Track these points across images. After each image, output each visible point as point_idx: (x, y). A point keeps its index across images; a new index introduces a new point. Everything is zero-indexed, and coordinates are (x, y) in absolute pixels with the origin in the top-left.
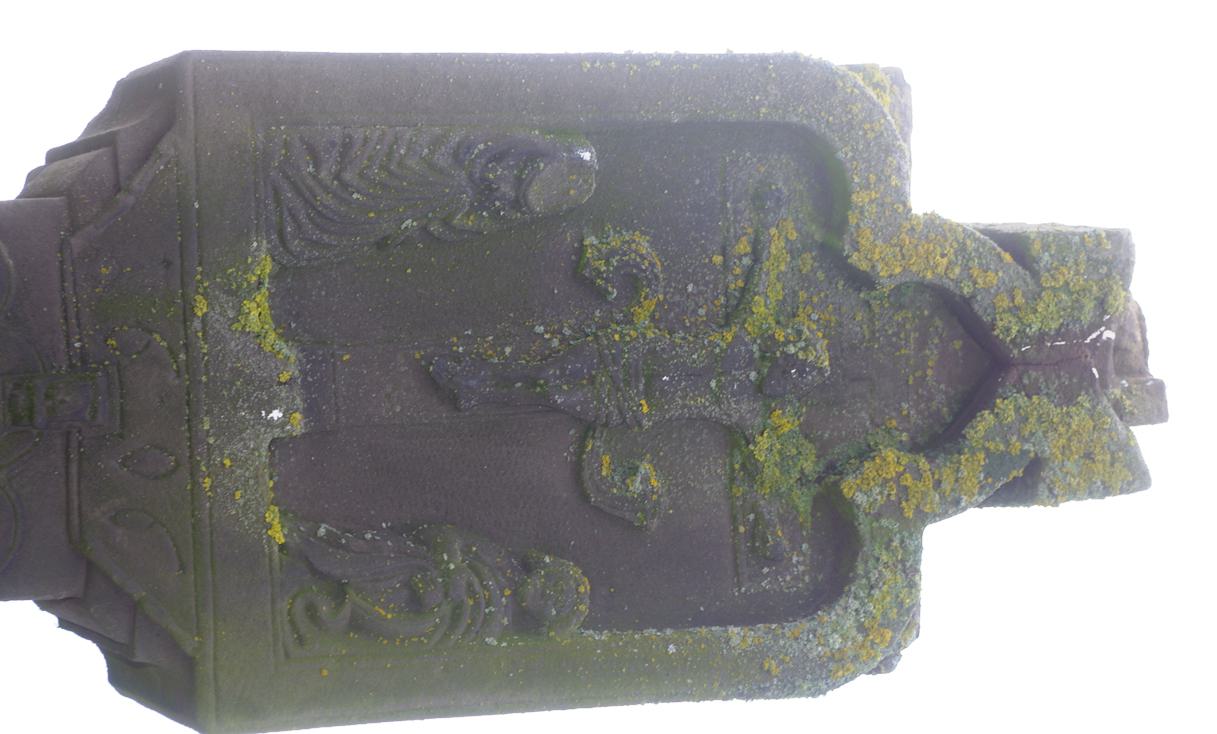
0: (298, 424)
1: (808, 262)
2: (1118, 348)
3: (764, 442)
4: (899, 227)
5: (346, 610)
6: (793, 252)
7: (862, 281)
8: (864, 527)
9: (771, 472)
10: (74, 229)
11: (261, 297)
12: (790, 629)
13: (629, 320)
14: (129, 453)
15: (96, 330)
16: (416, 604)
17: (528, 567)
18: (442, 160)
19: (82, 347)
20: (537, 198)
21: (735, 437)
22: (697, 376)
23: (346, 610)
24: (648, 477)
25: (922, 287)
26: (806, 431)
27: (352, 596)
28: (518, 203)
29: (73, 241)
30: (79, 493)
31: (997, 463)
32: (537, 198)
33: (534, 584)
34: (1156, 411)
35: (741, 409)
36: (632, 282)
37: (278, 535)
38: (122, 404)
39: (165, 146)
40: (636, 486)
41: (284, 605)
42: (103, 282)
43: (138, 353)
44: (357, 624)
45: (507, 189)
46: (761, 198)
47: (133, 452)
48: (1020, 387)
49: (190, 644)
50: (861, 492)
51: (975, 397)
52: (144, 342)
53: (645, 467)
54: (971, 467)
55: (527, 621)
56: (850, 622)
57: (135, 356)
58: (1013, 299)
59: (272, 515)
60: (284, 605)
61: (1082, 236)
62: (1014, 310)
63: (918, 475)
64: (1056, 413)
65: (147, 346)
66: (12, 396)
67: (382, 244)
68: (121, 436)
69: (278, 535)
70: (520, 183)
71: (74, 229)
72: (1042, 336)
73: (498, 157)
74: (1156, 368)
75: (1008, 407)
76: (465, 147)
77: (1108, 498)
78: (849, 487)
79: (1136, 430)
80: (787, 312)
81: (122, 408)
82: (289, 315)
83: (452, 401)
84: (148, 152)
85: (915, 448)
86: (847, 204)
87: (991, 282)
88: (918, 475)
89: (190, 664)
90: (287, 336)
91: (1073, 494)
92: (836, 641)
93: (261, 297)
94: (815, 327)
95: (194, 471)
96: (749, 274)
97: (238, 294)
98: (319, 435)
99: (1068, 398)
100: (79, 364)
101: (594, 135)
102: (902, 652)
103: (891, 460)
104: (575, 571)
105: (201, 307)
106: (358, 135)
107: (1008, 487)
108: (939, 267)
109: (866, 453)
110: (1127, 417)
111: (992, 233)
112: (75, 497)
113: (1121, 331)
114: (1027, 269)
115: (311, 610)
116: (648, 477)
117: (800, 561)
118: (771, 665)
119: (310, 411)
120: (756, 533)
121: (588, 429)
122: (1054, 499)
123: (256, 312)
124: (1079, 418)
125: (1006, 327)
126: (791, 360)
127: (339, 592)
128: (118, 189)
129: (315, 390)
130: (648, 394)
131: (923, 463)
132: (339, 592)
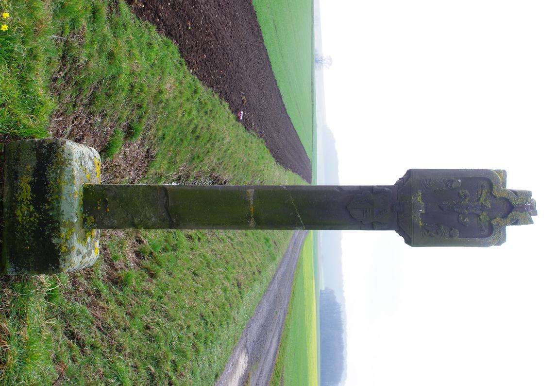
0: (424, 212)
1: (488, 194)
2: (531, 206)
3: (482, 216)
4: (212, 86)
5: (429, 234)
6: (486, 193)
7: (495, 197)
8: (494, 227)
9: (483, 220)
10: (399, 189)
11: (420, 197)
12: (484, 239)
13: (465, 201)
16: (437, 233)
17: (451, 230)
18: (442, 181)
20: (453, 186)
21: (478, 216)
22: (473, 208)
23: (429, 234)
24: (467, 220)
25: (504, 198)
26: (488, 215)
27: (430, 232)
28: (451, 187)
31: (512, 220)
32: (453, 186)
33: (451, 232)
34: (535, 213)
35: (479, 212)
36: (466, 196)
37: (421, 225)
39: (409, 180)
40: (465, 221)
41: (421, 233)
44: (430, 235)
45: (450, 185)
46: (482, 186)
48: (515, 210)
49: (410, 237)
50: (494, 222)
51: (510, 211)
53: (467, 218)
54: (508, 220)
55: (451, 236)
56: (492, 239)
59: (420, 222)
60: (421, 233)
61: (524, 192)
62: (514, 201)
63: (501, 221)
64: (520, 214)
67: (435, 191)
69: (421, 225)
70: (451, 184)
71: (399, 189)
72: (518, 204)
73: (449, 181)
74: (537, 209)
75: (514, 213)
76: (444, 180)
78: (492, 222)
79: (532, 216)
80: (485, 200)
82: (423, 200)
83: (442, 210)
84: (407, 180)
85: (502, 218)
86: (493, 187)
87: (512, 197)
88: (501, 221)
89: (410, 239)
90: (423, 201)
91: (522, 224)
92: (490, 241)
93: (420, 197)
94: (29, 203)
95: (411, 216)
96: (480, 195)
97: (417, 197)
98: (426, 213)
99: (522, 212)
101: (461, 179)
102: (510, 230)
103: (498, 219)
104: (457, 230)
105: (413, 198)
106: (431, 178)
107: (515, 223)
108: (505, 195)
109: (495, 218)
110: (530, 214)
111: (511, 190)
113: (531, 204)
115: (425, 233)
116: (467, 220)
117: (486, 231)
118: (482, 243)
119: (426, 210)
120: (481, 227)
121: (459, 214)
122: (520, 224)
123: (419, 198)
124: (523, 215)
125: (514, 203)
126: (485, 206)
127: (428, 231)
128: (404, 184)
129: (426, 208)
130: (467, 210)
131: (502, 219)
132: (428, 231)
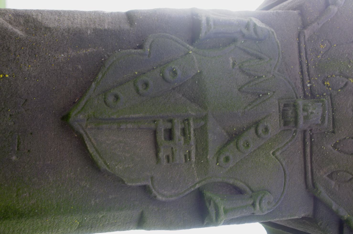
14: (338, 141)
15: (318, 77)
19: (310, 87)
29: (305, 31)
30: (311, 162)
38: (333, 115)
42: (322, 52)
43: (341, 88)
47: (340, 140)
52: (344, 83)
57: (339, 90)
58: (338, 183)
65: (346, 84)
66: (283, 110)
68: (333, 132)
77: (101, 10)
81: (333, 118)
100: (310, 95)
112: (309, 165)
114: (277, 221)
